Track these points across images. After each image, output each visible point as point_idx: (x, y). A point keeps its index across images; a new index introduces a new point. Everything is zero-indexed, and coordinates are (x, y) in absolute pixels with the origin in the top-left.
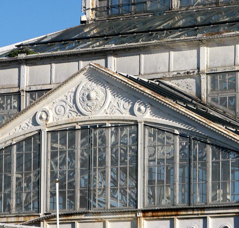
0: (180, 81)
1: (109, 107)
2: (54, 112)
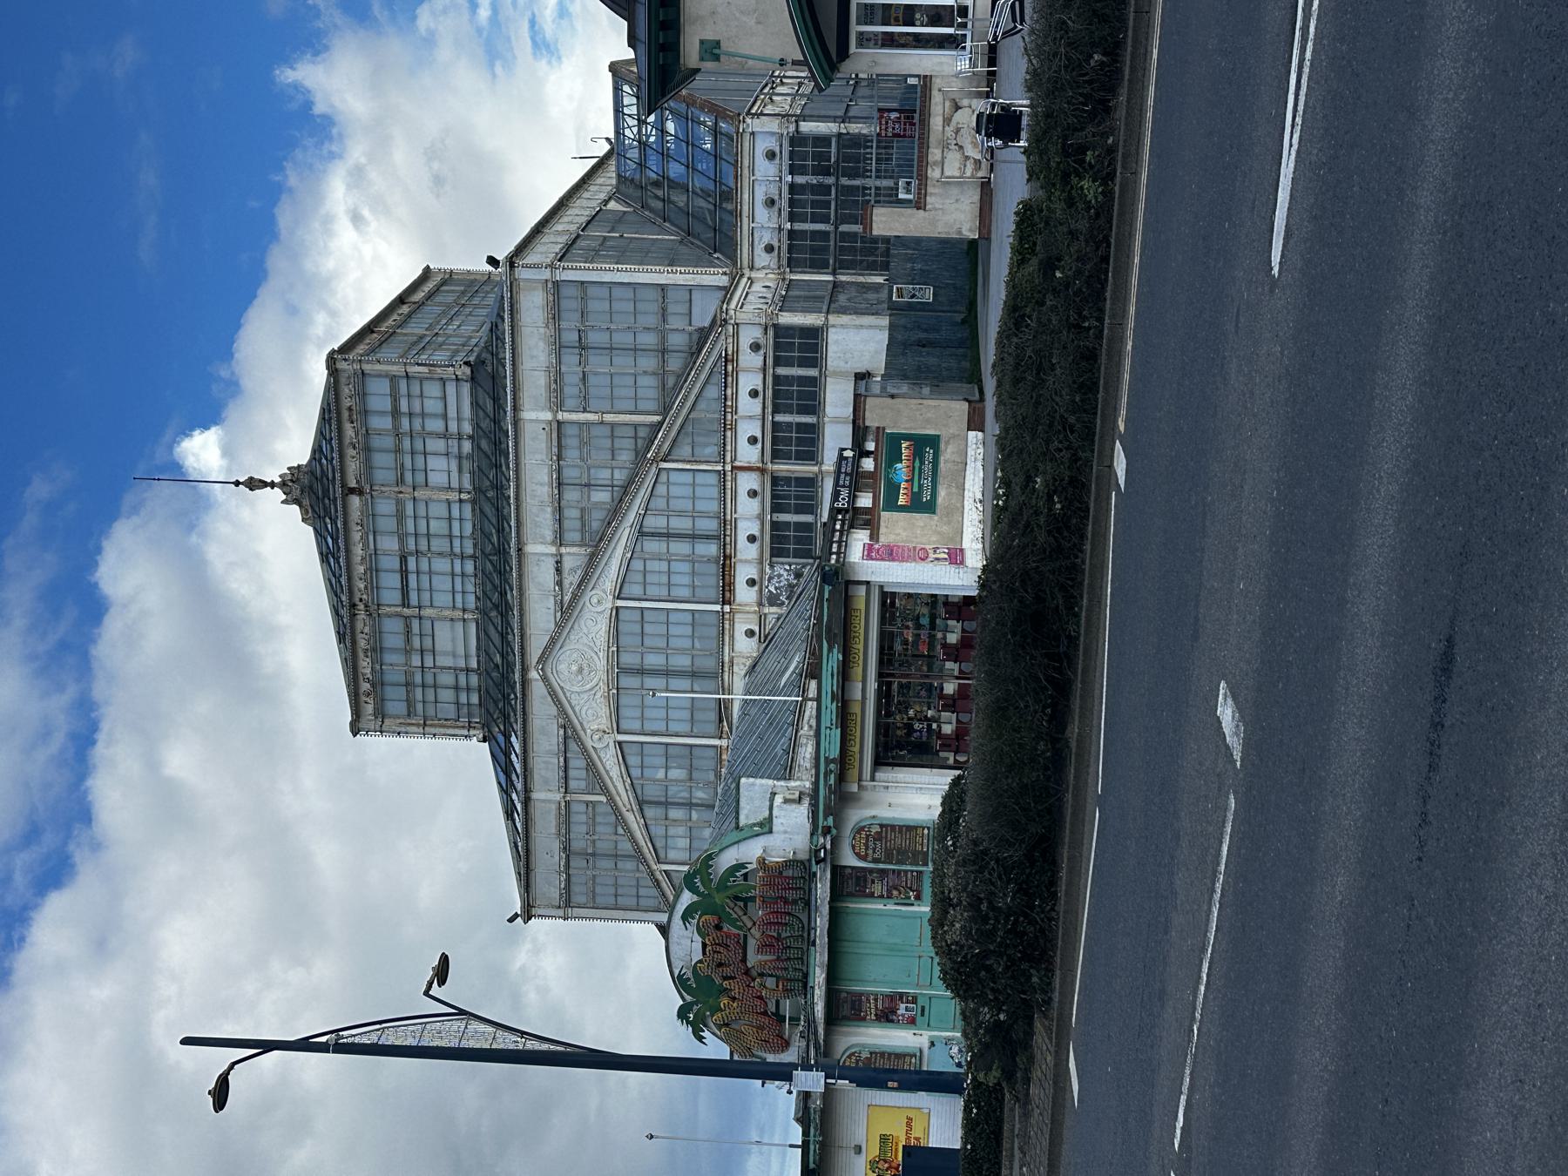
0: (566, 583)
1: (593, 627)
2: (593, 715)
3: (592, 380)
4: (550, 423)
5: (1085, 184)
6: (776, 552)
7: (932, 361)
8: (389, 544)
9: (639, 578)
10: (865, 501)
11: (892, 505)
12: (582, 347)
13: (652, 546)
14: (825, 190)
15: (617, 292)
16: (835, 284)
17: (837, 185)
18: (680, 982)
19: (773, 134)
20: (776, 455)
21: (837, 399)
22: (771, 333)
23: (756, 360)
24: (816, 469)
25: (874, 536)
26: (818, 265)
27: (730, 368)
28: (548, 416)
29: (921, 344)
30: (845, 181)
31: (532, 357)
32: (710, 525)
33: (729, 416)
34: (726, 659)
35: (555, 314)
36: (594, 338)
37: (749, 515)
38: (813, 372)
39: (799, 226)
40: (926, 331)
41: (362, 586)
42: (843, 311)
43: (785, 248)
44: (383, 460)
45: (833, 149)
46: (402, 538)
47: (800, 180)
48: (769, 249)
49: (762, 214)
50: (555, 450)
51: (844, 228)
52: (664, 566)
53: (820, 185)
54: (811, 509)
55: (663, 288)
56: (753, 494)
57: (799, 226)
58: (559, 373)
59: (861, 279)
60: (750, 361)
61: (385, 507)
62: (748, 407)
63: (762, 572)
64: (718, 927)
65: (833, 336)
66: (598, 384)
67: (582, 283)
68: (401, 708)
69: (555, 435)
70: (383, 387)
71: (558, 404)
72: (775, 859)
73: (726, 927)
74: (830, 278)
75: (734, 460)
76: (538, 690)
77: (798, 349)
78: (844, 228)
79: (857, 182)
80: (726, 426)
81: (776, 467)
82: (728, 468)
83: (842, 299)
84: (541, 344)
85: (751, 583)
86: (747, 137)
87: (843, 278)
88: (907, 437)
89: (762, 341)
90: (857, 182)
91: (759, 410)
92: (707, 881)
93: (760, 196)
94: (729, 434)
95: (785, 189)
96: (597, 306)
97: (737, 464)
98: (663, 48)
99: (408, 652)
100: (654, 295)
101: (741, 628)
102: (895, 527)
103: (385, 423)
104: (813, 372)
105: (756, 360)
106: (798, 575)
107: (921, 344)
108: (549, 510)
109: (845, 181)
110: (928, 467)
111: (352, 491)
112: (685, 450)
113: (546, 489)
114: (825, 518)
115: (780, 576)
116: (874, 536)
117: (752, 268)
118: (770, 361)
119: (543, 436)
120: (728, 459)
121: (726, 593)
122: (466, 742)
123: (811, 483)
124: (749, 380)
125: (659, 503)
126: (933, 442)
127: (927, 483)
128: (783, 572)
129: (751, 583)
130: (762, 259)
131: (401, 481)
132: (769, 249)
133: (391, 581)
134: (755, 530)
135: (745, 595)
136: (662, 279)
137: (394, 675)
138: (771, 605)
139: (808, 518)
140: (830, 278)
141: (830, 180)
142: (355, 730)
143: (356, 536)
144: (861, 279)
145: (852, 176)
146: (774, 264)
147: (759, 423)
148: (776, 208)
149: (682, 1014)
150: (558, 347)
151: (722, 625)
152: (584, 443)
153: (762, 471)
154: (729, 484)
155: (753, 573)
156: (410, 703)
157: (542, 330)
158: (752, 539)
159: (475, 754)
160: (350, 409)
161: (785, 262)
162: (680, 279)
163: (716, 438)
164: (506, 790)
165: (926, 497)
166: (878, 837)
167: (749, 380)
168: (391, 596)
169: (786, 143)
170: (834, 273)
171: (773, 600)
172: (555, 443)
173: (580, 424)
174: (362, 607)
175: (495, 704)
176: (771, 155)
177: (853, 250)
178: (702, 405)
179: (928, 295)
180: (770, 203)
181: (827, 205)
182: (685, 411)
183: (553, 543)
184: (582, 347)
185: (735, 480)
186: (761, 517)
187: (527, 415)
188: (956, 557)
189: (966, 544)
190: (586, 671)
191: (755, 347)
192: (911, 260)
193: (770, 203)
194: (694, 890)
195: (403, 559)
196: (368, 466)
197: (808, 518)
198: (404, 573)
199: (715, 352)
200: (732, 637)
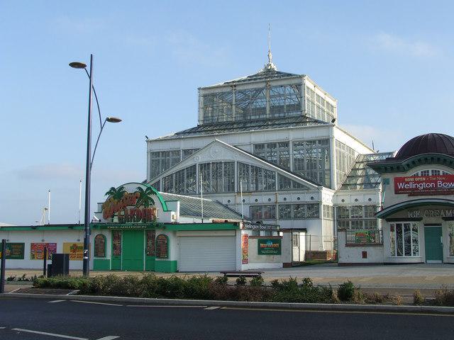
2: (200, 158)
5: (157, 234)
6: (251, 207)
10: (262, 234)
11: (260, 242)
18: (121, 188)
25: (251, 237)
54: (281, 218)
64: (137, 198)
72: (156, 212)
73: (137, 200)
76: (211, 140)
88: (280, 246)
92: (149, 194)
93: (270, 197)
98: (439, 159)
102: (254, 244)
110: (272, 252)
114: (264, 222)
116: (251, 237)
122: (197, 119)
123: (274, 217)
126: (279, 253)
127: (267, 252)
134: (302, 200)
142: (199, 89)
149: (113, 189)
159: (194, 123)
164: (184, 133)
165: (263, 252)
166: (164, 243)
175: (209, 127)
187: (291, 132)
188: (245, 261)
189: (250, 264)
194: (147, 190)
197: (350, 222)
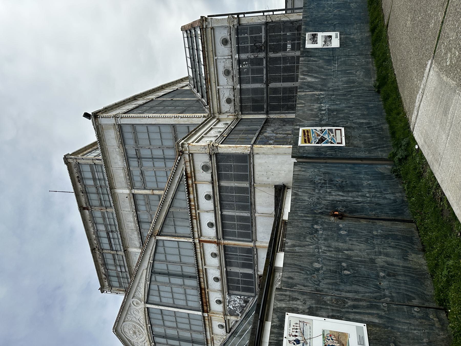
3: (146, 173)
4: (129, 194)
7: (359, 250)
8: (102, 228)
9: (157, 293)
12: (139, 158)
13: (160, 278)
14: (258, 61)
15: (151, 128)
16: (267, 121)
17: (266, 57)
19: (225, 27)
20: (225, 234)
21: (264, 202)
22: (214, 159)
23: (207, 176)
24: (252, 244)
26: (257, 109)
27: (190, 182)
28: (127, 191)
29: (342, 213)
30: (272, 55)
31: (115, 163)
32: (192, 270)
33: (193, 211)
34: (209, 338)
35: (123, 142)
36: (145, 153)
37: (213, 268)
38: (245, 185)
39: (244, 86)
40: (341, 188)
41: (96, 242)
42: (265, 142)
43: (237, 100)
44: (94, 197)
45: (263, 34)
46: (106, 226)
47: (244, 56)
48: (229, 101)
49: (223, 80)
50: (134, 207)
51: (272, 85)
52: (168, 289)
53: (256, 58)
55: (174, 126)
56: (214, 255)
57: (244, 86)
58: (129, 170)
59: (283, 116)
60: (204, 177)
61: (98, 214)
62: (206, 205)
63: (224, 298)
65: (258, 161)
66: (149, 174)
67: (133, 125)
68: (117, 284)
69: (132, 200)
70: (87, 168)
71: (132, 186)
74: (264, 116)
75: (201, 235)
77: (233, 171)
78: (272, 85)
79: (279, 55)
80: (194, 217)
81: (226, 242)
82: (197, 241)
83: (268, 132)
84: (118, 157)
85: (219, 302)
86: (209, 30)
87: (272, 116)
89: (209, 164)
90: (279, 55)
91: (212, 207)
93: (221, 70)
94: (195, 221)
95: (235, 63)
96: (143, 136)
97: (202, 239)
99: (116, 266)
100: (169, 130)
101: (215, 324)
103: (91, 182)
104: (245, 185)
105: (207, 176)
106: (246, 302)
107: (342, 213)
108: (136, 233)
109: (272, 55)
111: (84, 208)
112: (169, 229)
113: (133, 224)
115: (235, 301)
117: (220, 113)
118: (216, 177)
119: (127, 200)
120: (196, 236)
121: (205, 306)
124: (204, 189)
125: (160, 257)
128: (236, 300)
129: (219, 302)
130: (226, 107)
131: (101, 205)
132: (229, 101)
133: (105, 241)
135: (216, 308)
136: (172, 121)
137: (113, 273)
138: (231, 315)
139: (250, 271)
140: (264, 116)
141: (262, 55)
142: (102, 290)
143: (234, 145)
144: (283, 116)
145: (275, 51)
146: (232, 110)
147: (213, 215)
148: (231, 76)
150: (127, 158)
151: (206, 323)
152: (148, 204)
153: (218, 244)
154: (198, 250)
155: (219, 296)
156: (120, 283)
157: (117, 150)
158: (216, 279)
160: (78, 177)
161: (238, 108)
162: (182, 121)
163: (188, 223)
167: (204, 189)
168: (107, 246)
169: (233, 33)
170: (267, 113)
171: (232, 313)
172: (133, 204)
173: (144, 195)
174: (97, 249)
176: (225, 42)
177: (278, 99)
178: (176, 204)
179: (339, 137)
180: (227, 73)
181: (261, 71)
182: (166, 208)
183: (140, 248)
184: (139, 158)
185: (202, 247)
186: (220, 267)
190: (138, 333)
191: (205, 168)
192: (318, 100)
193: (227, 73)
195: (108, 234)
196: (88, 199)
197: (250, 271)
198: (109, 239)
199: (179, 172)
200: (211, 328)
